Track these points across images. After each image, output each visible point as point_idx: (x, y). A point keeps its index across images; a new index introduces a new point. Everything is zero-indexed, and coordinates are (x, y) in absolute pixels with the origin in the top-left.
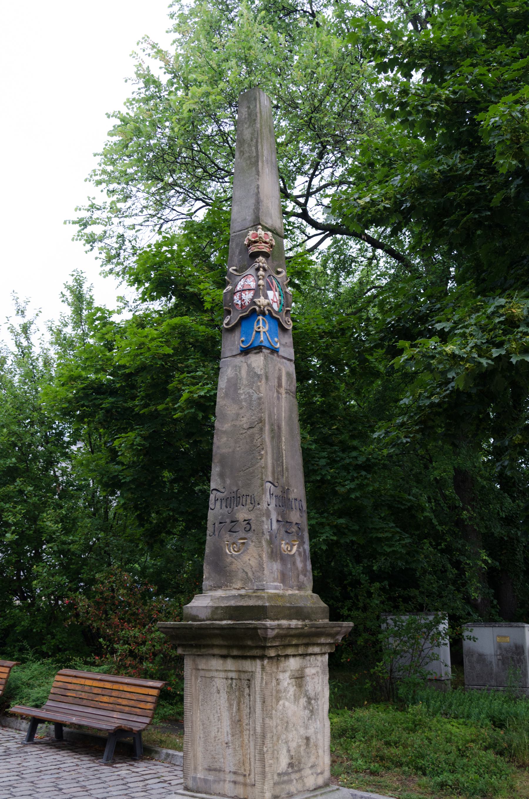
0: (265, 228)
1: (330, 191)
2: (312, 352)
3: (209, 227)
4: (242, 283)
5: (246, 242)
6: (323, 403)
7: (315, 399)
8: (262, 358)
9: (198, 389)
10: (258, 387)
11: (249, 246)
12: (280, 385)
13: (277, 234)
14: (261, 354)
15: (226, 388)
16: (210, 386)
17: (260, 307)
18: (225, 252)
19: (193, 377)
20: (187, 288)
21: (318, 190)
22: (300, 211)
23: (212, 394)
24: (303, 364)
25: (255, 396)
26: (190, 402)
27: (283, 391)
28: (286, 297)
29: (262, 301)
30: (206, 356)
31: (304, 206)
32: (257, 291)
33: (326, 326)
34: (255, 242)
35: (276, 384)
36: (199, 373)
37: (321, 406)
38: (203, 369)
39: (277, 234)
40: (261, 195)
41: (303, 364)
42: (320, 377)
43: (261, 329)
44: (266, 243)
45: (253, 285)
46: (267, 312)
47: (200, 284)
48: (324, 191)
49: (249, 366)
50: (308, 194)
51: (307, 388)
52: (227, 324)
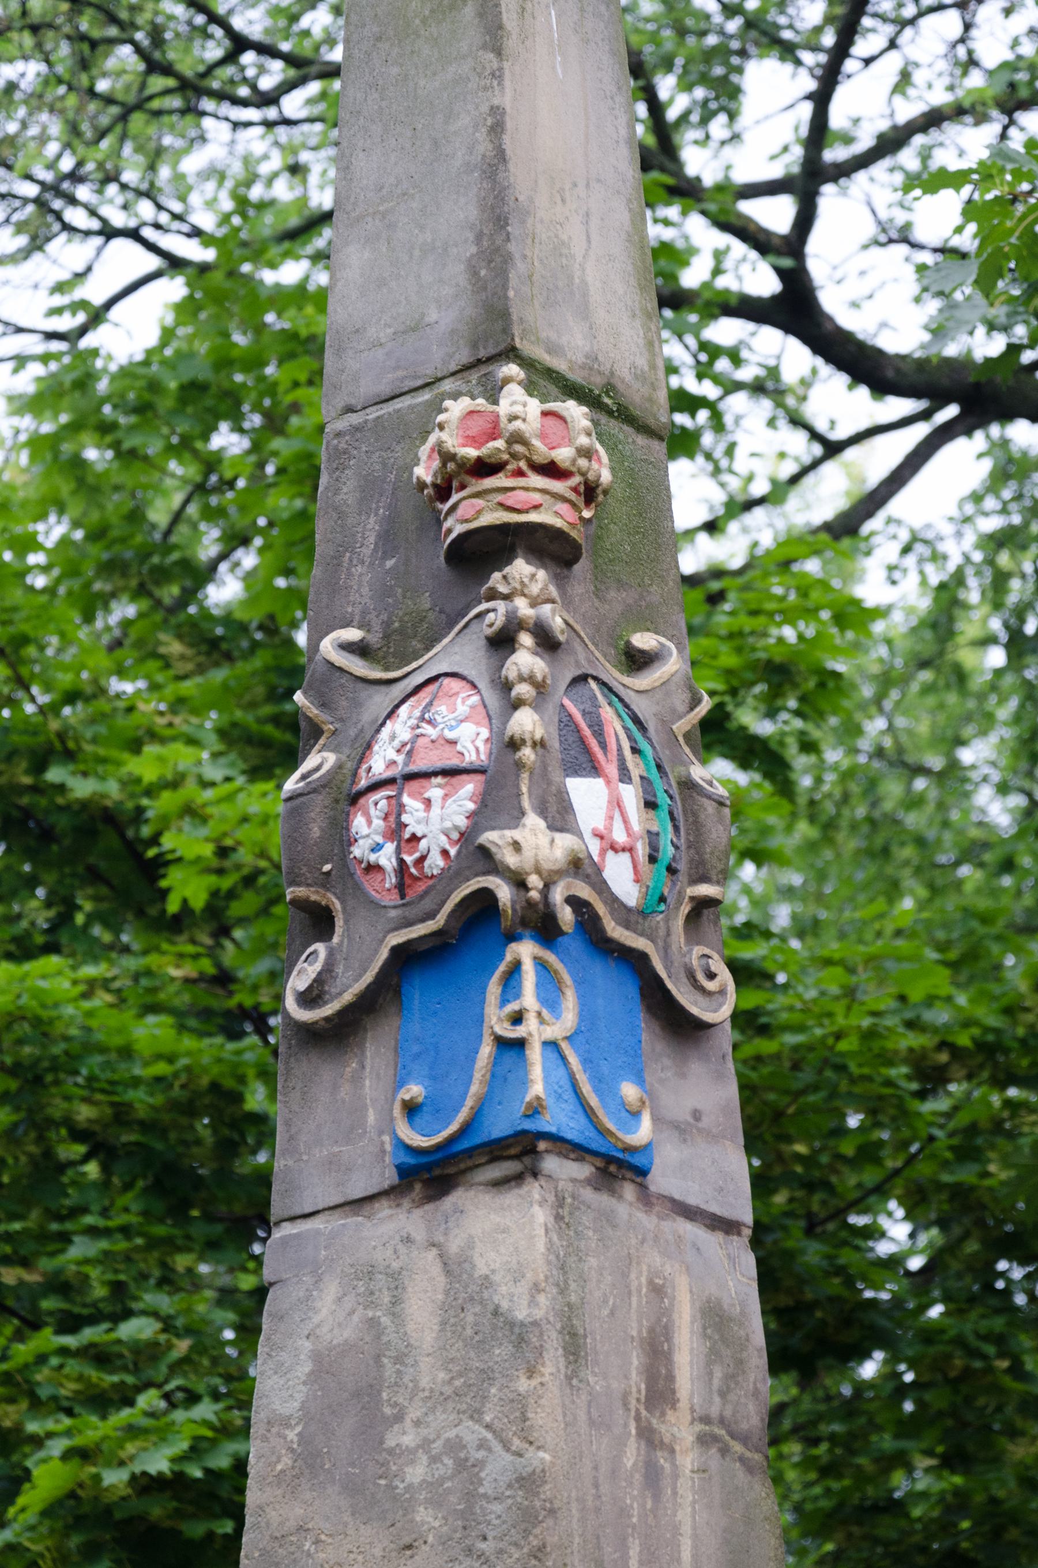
0: (547, 380)
1: (968, 145)
2: (870, 1176)
3: (192, 390)
4: (401, 727)
5: (424, 471)
6: (957, 1504)
7: (900, 1483)
8: (541, 1216)
9: (132, 1431)
10: (520, 1409)
11: (443, 491)
12: (659, 1392)
13: (625, 415)
14: (533, 1189)
15: (306, 1414)
16: (206, 1410)
17: (520, 884)
18: (295, 543)
19: (100, 1357)
20: (54, 774)
21: (890, 143)
22: (762, 280)
23: (221, 1461)
24: (813, 1253)
25: (498, 1468)
26: (79, 1522)
27: (680, 1428)
28: (696, 826)
29: (531, 843)
30: (178, 1211)
31: (788, 250)
32: (501, 776)
33: (957, 1008)
34: (484, 468)
35: (637, 1384)
36: (137, 1329)
37: (945, 1526)
38: (163, 1301)
39: (625, 415)
40: (519, 175)
41: (813, 1253)
42: (930, 1335)
43: (530, 1027)
44: (551, 470)
45: (473, 741)
46: (566, 915)
47: (135, 746)
48: (925, 156)
49: (454, 1268)
50: (810, 179)
51: (850, 1409)
52: (310, 998)
